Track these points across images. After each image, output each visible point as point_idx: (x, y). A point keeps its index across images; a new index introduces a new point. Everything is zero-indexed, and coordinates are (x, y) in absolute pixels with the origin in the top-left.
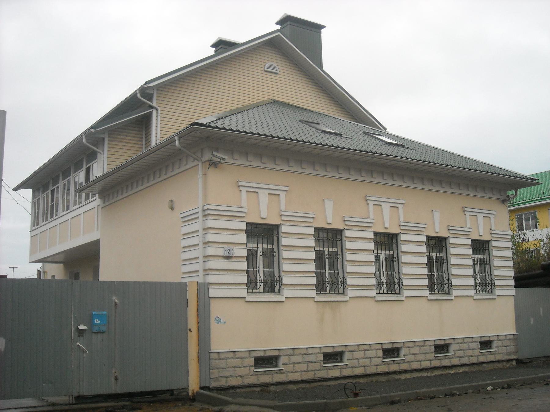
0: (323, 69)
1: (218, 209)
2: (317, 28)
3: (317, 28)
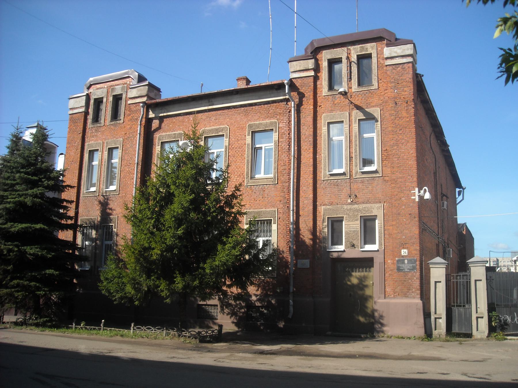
0: (457, 206)
1: (77, 171)
2: (251, 82)
3: (251, 82)
